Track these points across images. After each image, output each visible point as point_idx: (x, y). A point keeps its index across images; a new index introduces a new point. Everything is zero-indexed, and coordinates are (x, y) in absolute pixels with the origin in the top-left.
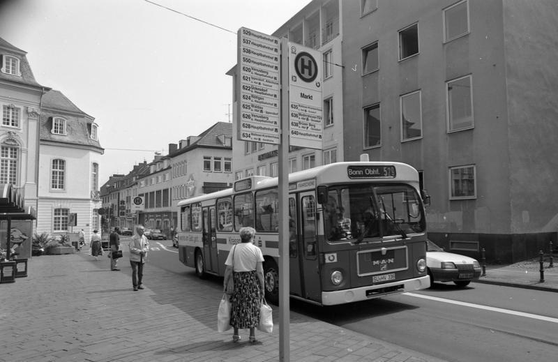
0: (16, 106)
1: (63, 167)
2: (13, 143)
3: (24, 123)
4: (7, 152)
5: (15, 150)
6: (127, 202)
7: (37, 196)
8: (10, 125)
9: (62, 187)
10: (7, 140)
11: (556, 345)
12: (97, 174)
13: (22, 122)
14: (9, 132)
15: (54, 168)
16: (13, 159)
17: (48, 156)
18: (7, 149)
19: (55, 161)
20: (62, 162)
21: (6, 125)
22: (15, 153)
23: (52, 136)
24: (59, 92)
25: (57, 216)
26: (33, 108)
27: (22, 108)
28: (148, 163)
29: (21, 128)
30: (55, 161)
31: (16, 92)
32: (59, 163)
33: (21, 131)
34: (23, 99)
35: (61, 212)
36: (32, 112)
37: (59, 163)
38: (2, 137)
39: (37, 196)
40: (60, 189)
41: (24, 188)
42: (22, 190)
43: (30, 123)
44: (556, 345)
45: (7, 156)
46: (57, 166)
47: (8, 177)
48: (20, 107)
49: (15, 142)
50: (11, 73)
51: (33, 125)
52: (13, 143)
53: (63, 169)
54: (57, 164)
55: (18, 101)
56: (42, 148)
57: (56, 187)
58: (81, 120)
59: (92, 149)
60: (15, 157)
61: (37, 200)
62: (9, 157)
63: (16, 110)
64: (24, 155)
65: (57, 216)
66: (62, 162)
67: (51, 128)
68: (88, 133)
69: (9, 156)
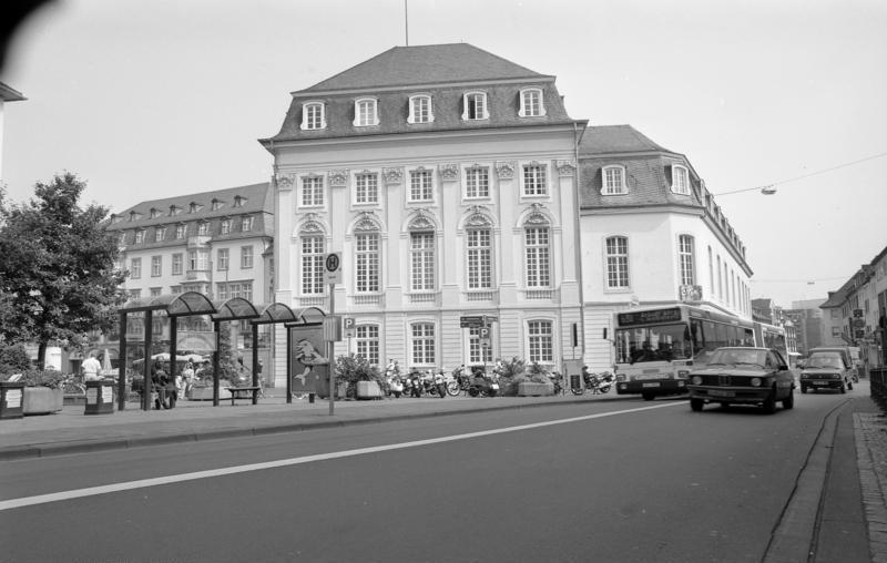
0: (541, 162)
1: (625, 249)
2: (539, 221)
3: (554, 187)
4: (534, 237)
5: (546, 231)
6: (867, 311)
7: (581, 301)
8: (536, 194)
9: (625, 283)
10: (531, 218)
11: (763, 560)
12: (694, 254)
13: (550, 184)
14: (533, 205)
15: (609, 252)
16: (543, 245)
17: (596, 233)
18: (533, 231)
19: (610, 241)
20: (623, 241)
21: (416, 200)
22: (546, 236)
23: (603, 200)
24: (628, 127)
25: (534, 335)
26: (567, 158)
27: (549, 163)
28: (83, 203)
29: (550, 195)
30: (610, 241)
31: (335, 153)
32: (617, 243)
33: (549, 200)
34: (487, 151)
35: (540, 328)
36: (564, 167)
37: (617, 243)
38: (525, 214)
39: (581, 301)
40: (623, 288)
41: (559, 290)
42: (557, 293)
43: (562, 184)
44: (763, 560)
45: (534, 242)
46: (614, 249)
47: (480, 277)
48: (545, 162)
49: (483, 219)
50: (532, 115)
51: (567, 187)
52: (539, 221)
53: (625, 252)
54: (614, 244)
55: (485, 156)
56: (584, 222)
57: (616, 285)
58: (652, 163)
59: (674, 209)
60: (546, 242)
61: (581, 308)
62: (537, 244)
63: (484, 171)
64: (556, 237)
65: (534, 335)
66: (623, 241)
67: (601, 186)
68: (666, 182)
69: (537, 242)
